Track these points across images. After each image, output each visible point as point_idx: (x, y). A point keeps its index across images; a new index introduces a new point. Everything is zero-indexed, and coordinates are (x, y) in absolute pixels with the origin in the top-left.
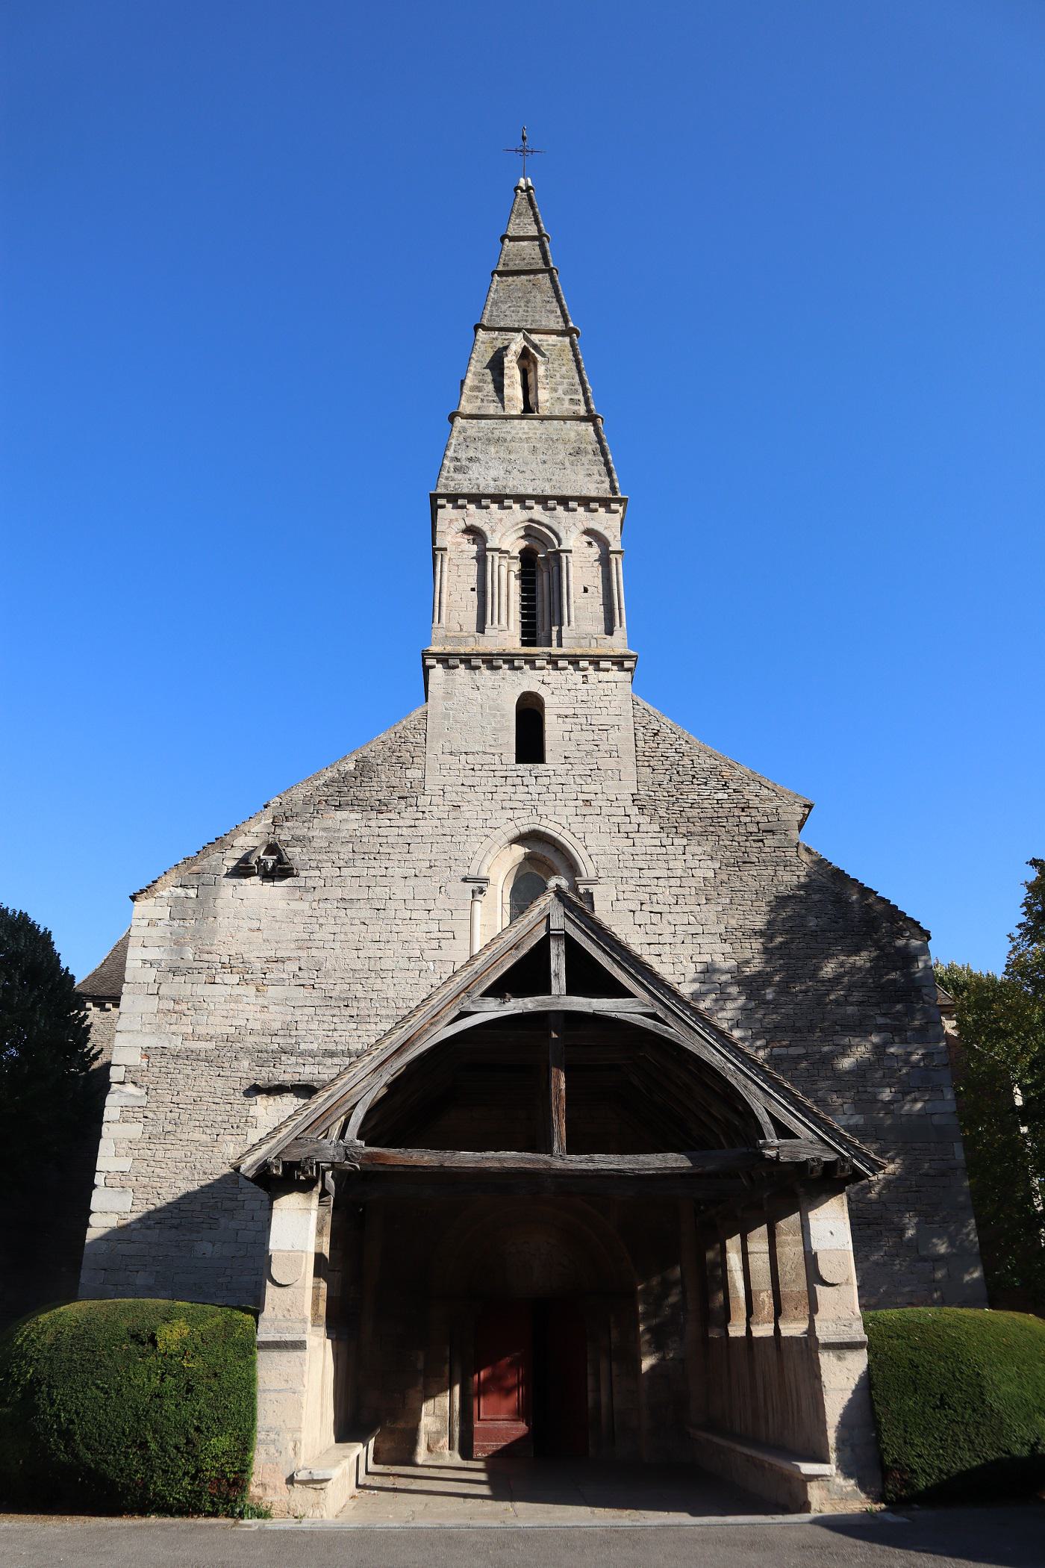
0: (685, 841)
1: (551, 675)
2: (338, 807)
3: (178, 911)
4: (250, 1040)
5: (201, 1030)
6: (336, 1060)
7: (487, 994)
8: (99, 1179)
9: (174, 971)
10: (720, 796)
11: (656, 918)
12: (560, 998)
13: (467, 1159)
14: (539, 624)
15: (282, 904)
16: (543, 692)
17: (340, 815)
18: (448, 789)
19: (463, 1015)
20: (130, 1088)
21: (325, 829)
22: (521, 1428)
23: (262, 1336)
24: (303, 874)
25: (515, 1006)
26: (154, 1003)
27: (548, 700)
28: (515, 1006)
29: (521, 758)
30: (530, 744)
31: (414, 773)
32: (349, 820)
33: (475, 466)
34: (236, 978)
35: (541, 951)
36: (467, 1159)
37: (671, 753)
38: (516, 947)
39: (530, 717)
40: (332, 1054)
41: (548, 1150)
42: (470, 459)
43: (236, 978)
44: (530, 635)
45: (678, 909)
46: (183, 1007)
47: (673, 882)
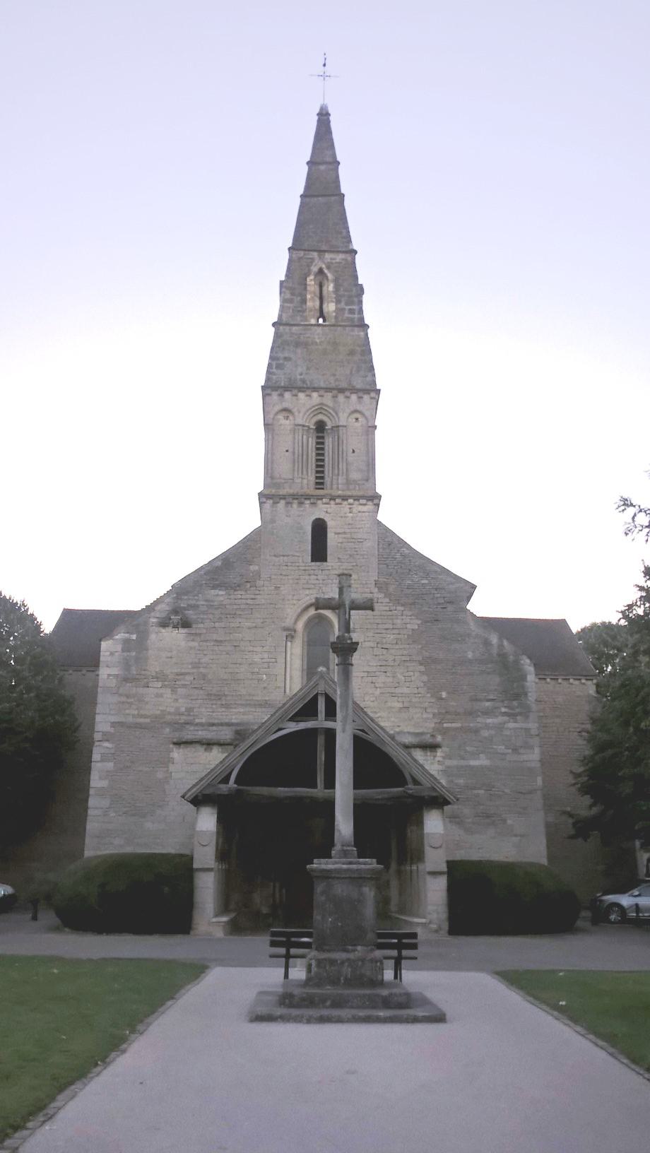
4: (168, 718)
5: (142, 712)
8: (92, 792)
9: (126, 680)
10: (425, 581)
15: (183, 644)
20: (106, 744)
22: (48, 624)
23: (195, 866)
26: (115, 699)
27: (330, 523)
28: (302, 726)
30: (319, 552)
32: (219, 595)
33: (288, 364)
34: (160, 684)
37: (398, 556)
39: (319, 529)
41: (315, 786)
42: (285, 359)
43: (160, 684)
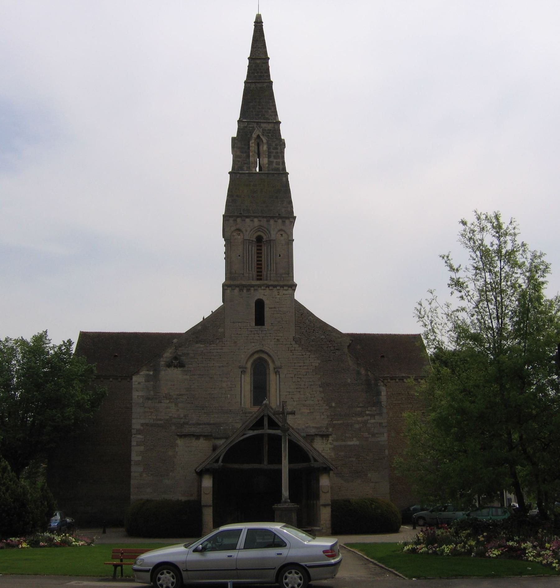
0: (309, 353)
1: (267, 292)
2: (197, 343)
3: (148, 378)
6: (201, 426)
7: (249, 430)
9: (148, 399)
10: (322, 337)
11: (299, 380)
12: (267, 431)
13: (246, 466)
14: (263, 268)
16: (264, 298)
17: (197, 345)
18: (233, 335)
19: (244, 434)
21: (193, 350)
24: (187, 366)
25: (256, 432)
27: (266, 302)
28: (256, 432)
29: (257, 324)
30: (260, 320)
31: (221, 330)
34: (168, 401)
35: (262, 419)
36: (246, 466)
38: (256, 418)
40: (199, 424)
44: (259, 277)
45: (306, 377)
46: (152, 410)
47: (306, 367)
